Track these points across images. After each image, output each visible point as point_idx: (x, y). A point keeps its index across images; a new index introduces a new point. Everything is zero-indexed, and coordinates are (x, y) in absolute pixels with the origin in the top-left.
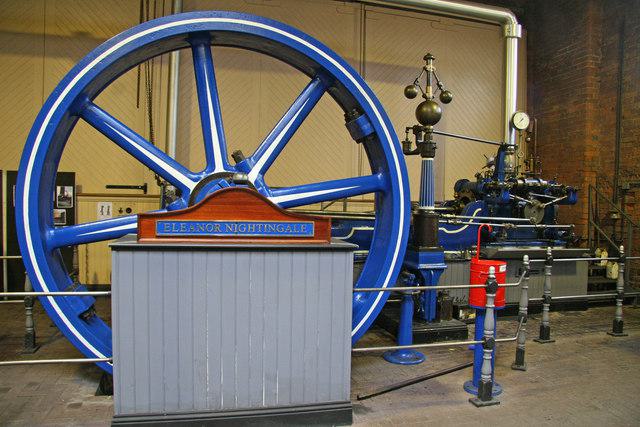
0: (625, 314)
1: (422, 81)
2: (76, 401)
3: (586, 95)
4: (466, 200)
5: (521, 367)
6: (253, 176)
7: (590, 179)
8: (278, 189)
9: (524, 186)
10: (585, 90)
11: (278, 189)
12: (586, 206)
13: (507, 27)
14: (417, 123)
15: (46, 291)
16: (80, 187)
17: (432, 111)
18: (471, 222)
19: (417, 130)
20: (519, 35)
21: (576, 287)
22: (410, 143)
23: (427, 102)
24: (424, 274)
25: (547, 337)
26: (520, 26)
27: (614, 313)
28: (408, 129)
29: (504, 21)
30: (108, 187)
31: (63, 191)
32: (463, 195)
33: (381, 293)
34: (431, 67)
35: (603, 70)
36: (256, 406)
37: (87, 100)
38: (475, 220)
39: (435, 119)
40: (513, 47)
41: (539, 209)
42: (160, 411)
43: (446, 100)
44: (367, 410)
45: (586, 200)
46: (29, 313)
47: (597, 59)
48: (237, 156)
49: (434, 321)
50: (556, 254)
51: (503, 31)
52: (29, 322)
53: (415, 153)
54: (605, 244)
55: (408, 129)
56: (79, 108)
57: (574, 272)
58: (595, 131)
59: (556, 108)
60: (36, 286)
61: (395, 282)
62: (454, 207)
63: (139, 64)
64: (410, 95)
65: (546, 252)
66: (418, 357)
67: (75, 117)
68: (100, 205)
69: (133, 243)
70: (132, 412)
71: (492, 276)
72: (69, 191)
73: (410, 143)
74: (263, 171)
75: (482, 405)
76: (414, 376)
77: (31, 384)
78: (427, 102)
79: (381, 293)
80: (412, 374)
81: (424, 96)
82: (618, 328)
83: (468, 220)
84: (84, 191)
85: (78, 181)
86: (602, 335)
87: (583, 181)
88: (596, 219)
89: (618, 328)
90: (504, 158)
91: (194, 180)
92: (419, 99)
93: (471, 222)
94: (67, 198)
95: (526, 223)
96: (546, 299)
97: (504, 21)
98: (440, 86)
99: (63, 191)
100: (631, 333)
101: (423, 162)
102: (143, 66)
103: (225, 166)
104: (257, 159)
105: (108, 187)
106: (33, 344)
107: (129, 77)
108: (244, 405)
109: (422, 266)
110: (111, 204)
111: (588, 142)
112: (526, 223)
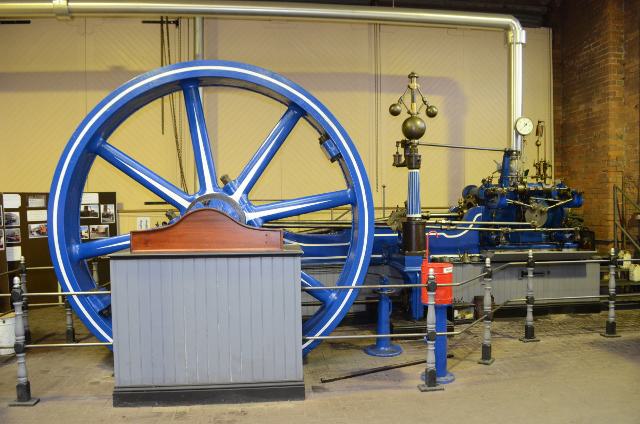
0: (617, 315)
1: (408, 99)
2: (96, 380)
3: (608, 94)
4: (469, 205)
5: (487, 361)
6: (237, 196)
7: (615, 179)
8: (284, 201)
9: (524, 191)
10: (608, 89)
11: (284, 201)
12: (611, 206)
13: (511, 34)
14: (404, 138)
15: (72, 292)
16: (121, 205)
17: (416, 126)
18: (470, 227)
19: (405, 144)
20: (524, 41)
21: (585, 288)
22: (400, 156)
23: (412, 118)
24: (411, 276)
25: (533, 335)
26: (524, 32)
27: (607, 316)
28: (398, 143)
29: (507, 28)
30: (147, 203)
31: (105, 209)
32: (469, 200)
33: (351, 291)
34: (415, 85)
35: (627, 66)
36: (226, 382)
37: (101, 139)
38: (475, 225)
39: (419, 134)
40: (518, 53)
41: (542, 212)
42: (151, 384)
43: (431, 115)
44: (324, 390)
45: (611, 201)
46: (69, 313)
47: (620, 56)
48: (224, 180)
49: (420, 320)
50: (537, 257)
51: (506, 38)
52: (69, 321)
53: (403, 165)
54: (476, 242)
55: (398, 143)
56: (94, 148)
57: (583, 274)
58: (619, 131)
59: (582, 107)
60: (65, 288)
61: (363, 280)
62: (458, 214)
63: (162, 96)
64: (395, 113)
65: (527, 255)
66: (399, 351)
67: (179, 87)
68: (139, 219)
69: (127, 253)
70: (128, 384)
71: (431, 277)
72: (111, 209)
73: (400, 156)
74: (247, 191)
75: (425, 391)
76: (382, 365)
77: (66, 368)
78: (412, 118)
79: (351, 291)
80: (379, 363)
81: (409, 113)
82: (611, 329)
83: (469, 225)
84: (125, 208)
85: (119, 199)
86: (595, 336)
87: (608, 182)
88: (622, 221)
89: (611, 329)
90: (509, 163)
91: (189, 200)
92: (404, 116)
93: (470, 227)
94: (108, 216)
95: (529, 227)
96: (530, 300)
97: (507, 28)
98: (425, 102)
99: (105, 209)
100: (625, 335)
101: (411, 174)
102: (166, 97)
103: (215, 186)
104: (240, 182)
105: (147, 203)
106: (71, 336)
107: (155, 105)
108: (216, 381)
109: (408, 269)
110: (148, 219)
111: (612, 141)
112: (529, 227)
